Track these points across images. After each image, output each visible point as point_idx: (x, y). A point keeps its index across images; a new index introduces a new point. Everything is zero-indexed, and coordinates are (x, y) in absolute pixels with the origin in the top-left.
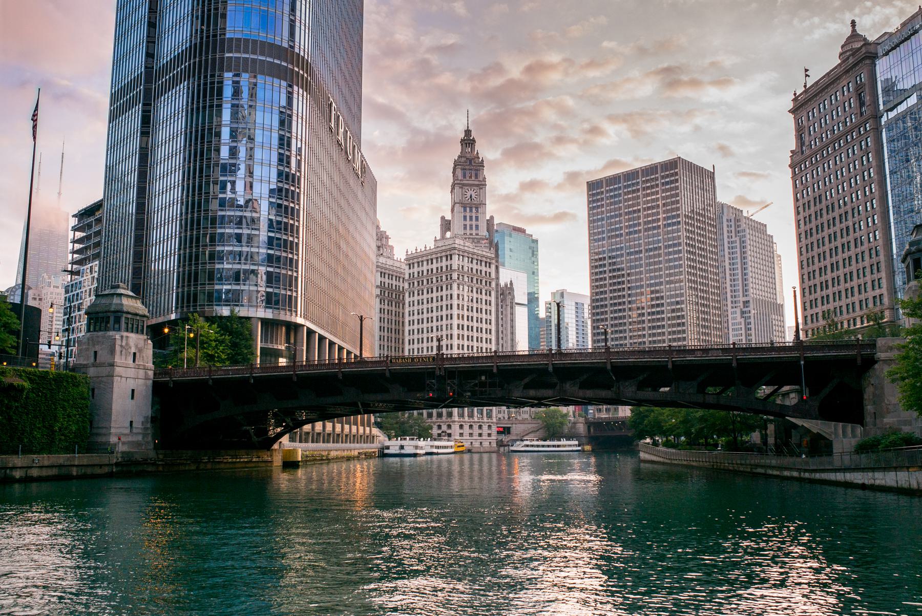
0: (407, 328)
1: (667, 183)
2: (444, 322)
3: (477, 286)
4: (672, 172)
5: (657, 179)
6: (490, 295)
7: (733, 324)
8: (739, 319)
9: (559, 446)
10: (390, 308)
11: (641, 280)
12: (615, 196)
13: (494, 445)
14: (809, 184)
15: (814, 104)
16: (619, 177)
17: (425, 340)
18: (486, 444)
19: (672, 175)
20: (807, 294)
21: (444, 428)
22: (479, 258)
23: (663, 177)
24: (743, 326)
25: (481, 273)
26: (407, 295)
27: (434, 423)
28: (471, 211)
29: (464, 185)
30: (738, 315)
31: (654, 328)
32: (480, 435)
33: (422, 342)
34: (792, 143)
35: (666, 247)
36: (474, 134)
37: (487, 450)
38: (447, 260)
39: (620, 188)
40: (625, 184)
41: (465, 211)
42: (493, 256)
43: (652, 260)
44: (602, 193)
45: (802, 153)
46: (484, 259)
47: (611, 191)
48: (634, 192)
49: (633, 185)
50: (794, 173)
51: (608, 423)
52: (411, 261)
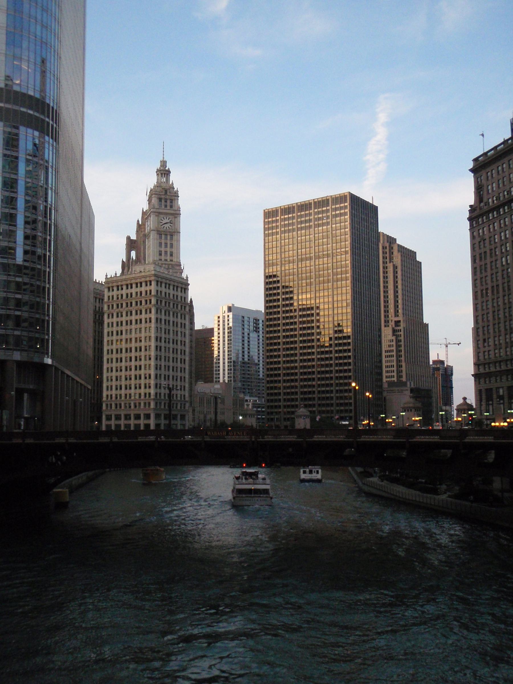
3: (174, 310)
6: (185, 319)
14: (487, 237)
15: (494, 166)
17: (114, 360)
20: (478, 273)
22: (168, 282)
25: (177, 298)
26: (106, 316)
28: (166, 239)
29: (160, 213)
30: (390, 332)
36: (169, 166)
38: (147, 285)
41: (161, 238)
45: (480, 209)
46: (164, 281)
50: (471, 225)
52: (110, 285)
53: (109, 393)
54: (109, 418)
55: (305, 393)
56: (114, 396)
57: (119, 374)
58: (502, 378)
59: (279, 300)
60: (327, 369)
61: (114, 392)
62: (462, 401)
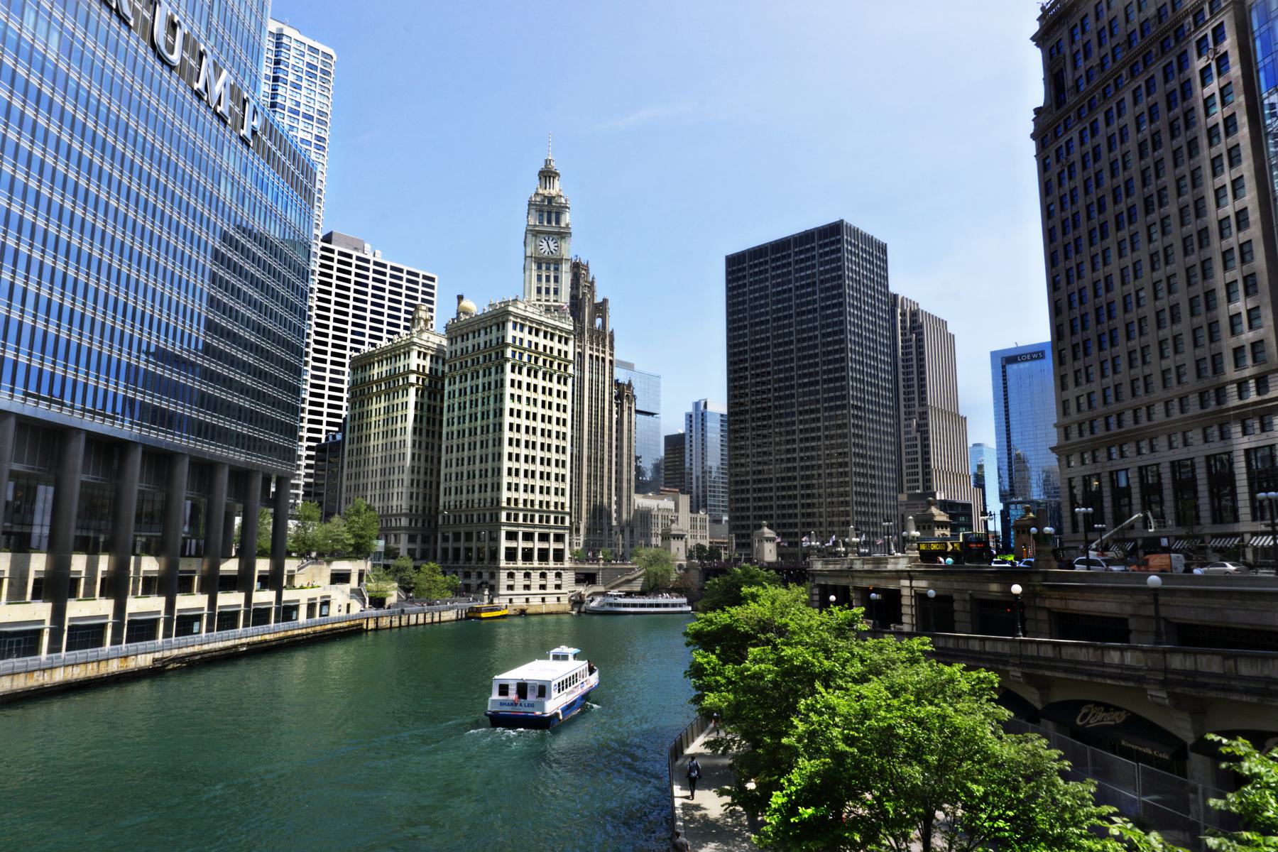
1: (826, 254)
5: (813, 248)
6: (565, 384)
7: (908, 440)
8: (914, 434)
9: (658, 605)
10: (432, 403)
11: (792, 378)
12: (761, 272)
19: (832, 243)
21: (486, 576)
23: (821, 247)
24: (919, 442)
27: (474, 569)
28: (548, 269)
31: (807, 440)
32: (543, 587)
34: (1037, 95)
35: (824, 336)
37: (554, 609)
39: (766, 262)
41: (539, 268)
42: (572, 328)
47: (756, 266)
48: (784, 266)
54: (445, 539)
55: (784, 507)
58: (1125, 448)
62: (1054, 456)
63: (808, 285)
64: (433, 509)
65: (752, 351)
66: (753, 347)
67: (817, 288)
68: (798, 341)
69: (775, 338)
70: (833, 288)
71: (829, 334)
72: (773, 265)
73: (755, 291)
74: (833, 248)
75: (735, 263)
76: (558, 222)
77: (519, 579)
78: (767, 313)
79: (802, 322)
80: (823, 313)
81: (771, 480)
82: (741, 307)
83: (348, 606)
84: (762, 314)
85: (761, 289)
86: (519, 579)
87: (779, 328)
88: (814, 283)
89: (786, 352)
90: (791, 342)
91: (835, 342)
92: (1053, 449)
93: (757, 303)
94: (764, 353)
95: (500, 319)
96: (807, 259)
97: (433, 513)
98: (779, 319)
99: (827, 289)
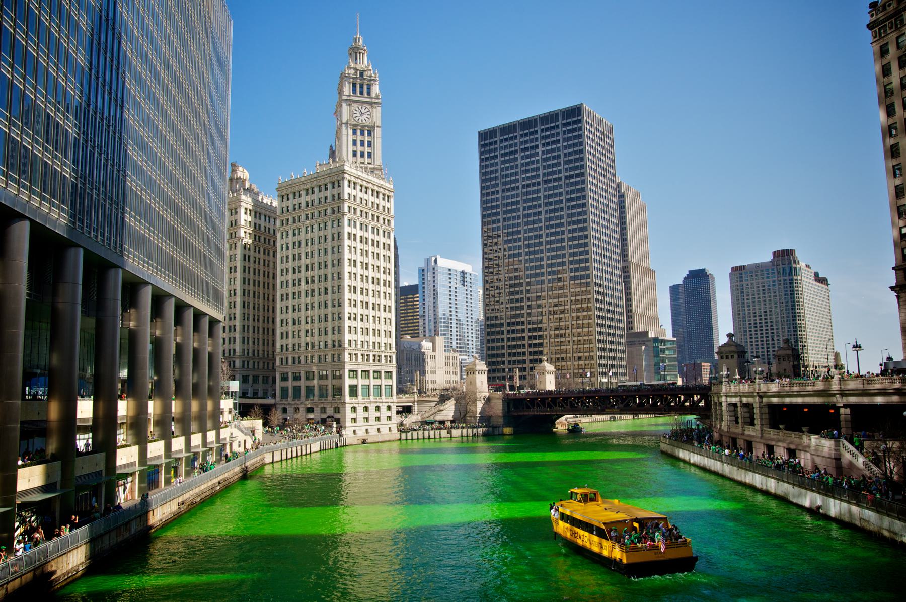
0: (279, 279)
2: (329, 270)
4: (574, 119)
13: (395, 430)
16: (515, 125)
18: (384, 430)
19: (574, 123)
21: (330, 411)
23: (564, 125)
26: (279, 235)
28: (362, 134)
33: (287, 337)
35: (568, 200)
40: (521, 133)
41: (355, 133)
43: (531, 226)
44: (496, 142)
49: (531, 133)
51: (532, 400)
53: (284, 342)
54: (285, 378)
56: (290, 346)
57: (296, 315)
59: (524, 346)
60: (514, 207)
61: (290, 341)
63: (554, 158)
64: (270, 353)
65: (504, 213)
66: (505, 209)
67: (561, 160)
68: (546, 204)
69: (524, 202)
70: (576, 160)
71: (573, 199)
72: (522, 140)
73: (506, 162)
74: (575, 126)
75: (486, 137)
76: (369, 93)
77: (360, 414)
78: (517, 180)
79: (549, 189)
80: (567, 181)
81: (502, 325)
82: (493, 175)
83: (245, 441)
84: (513, 182)
85: (511, 160)
86: (360, 414)
87: (528, 193)
88: (559, 156)
89: (535, 214)
90: (539, 206)
91: (579, 206)
92: (892, 288)
93: (508, 172)
94: (514, 215)
95: (335, 178)
96: (553, 136)
97: (270, 356)
98: (528, 186)
99: (571, 161)
